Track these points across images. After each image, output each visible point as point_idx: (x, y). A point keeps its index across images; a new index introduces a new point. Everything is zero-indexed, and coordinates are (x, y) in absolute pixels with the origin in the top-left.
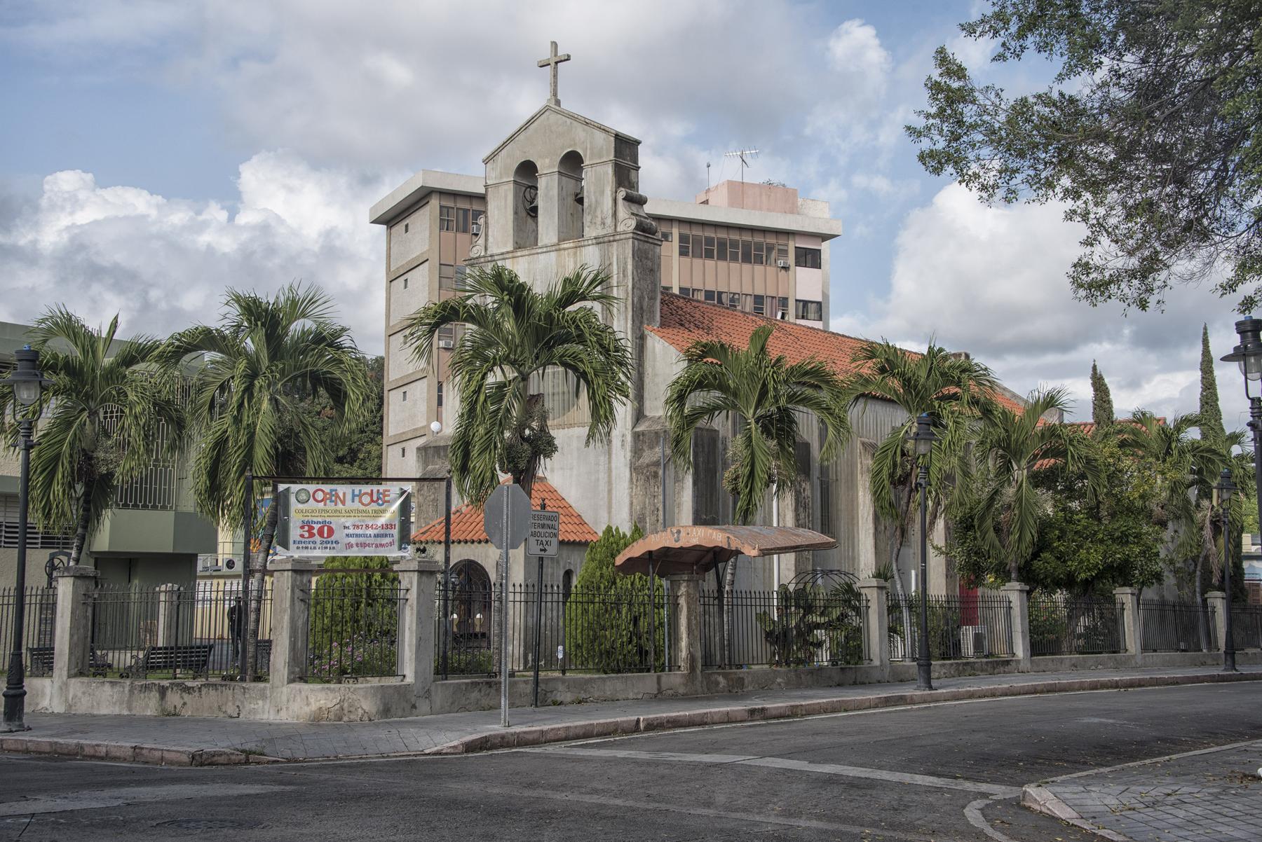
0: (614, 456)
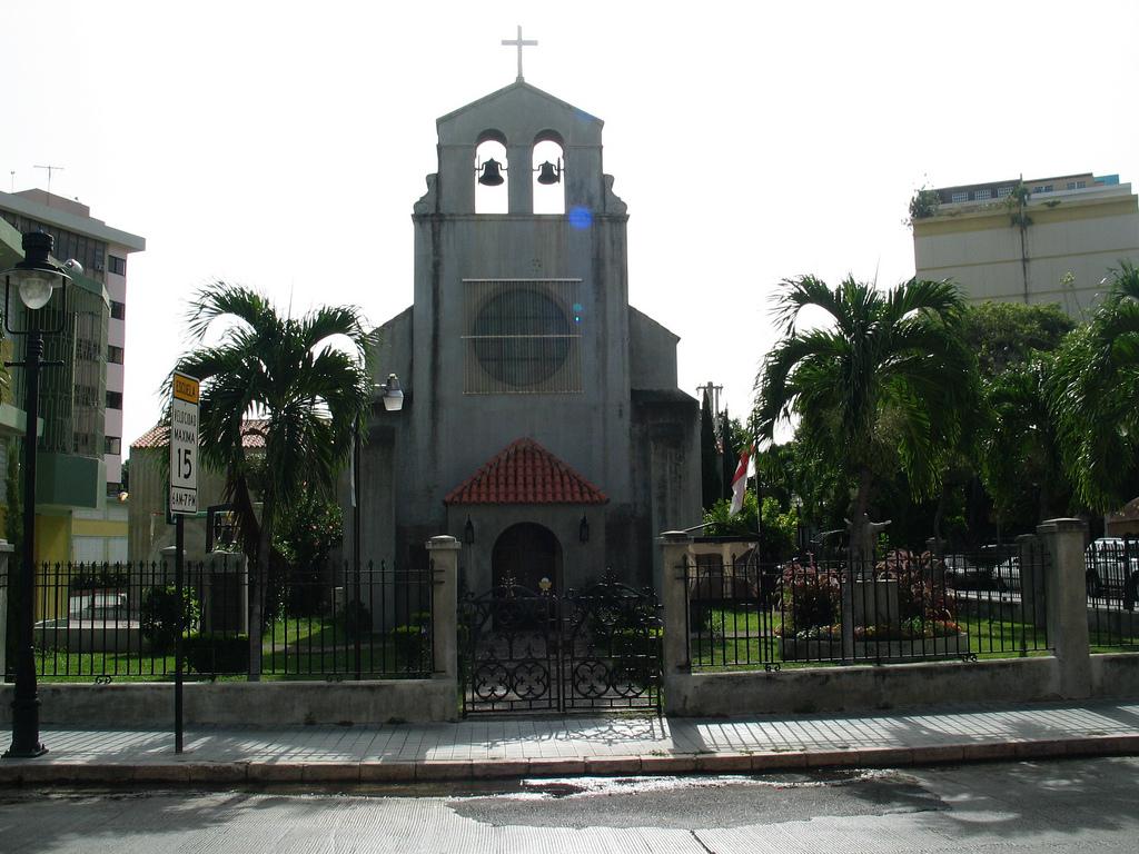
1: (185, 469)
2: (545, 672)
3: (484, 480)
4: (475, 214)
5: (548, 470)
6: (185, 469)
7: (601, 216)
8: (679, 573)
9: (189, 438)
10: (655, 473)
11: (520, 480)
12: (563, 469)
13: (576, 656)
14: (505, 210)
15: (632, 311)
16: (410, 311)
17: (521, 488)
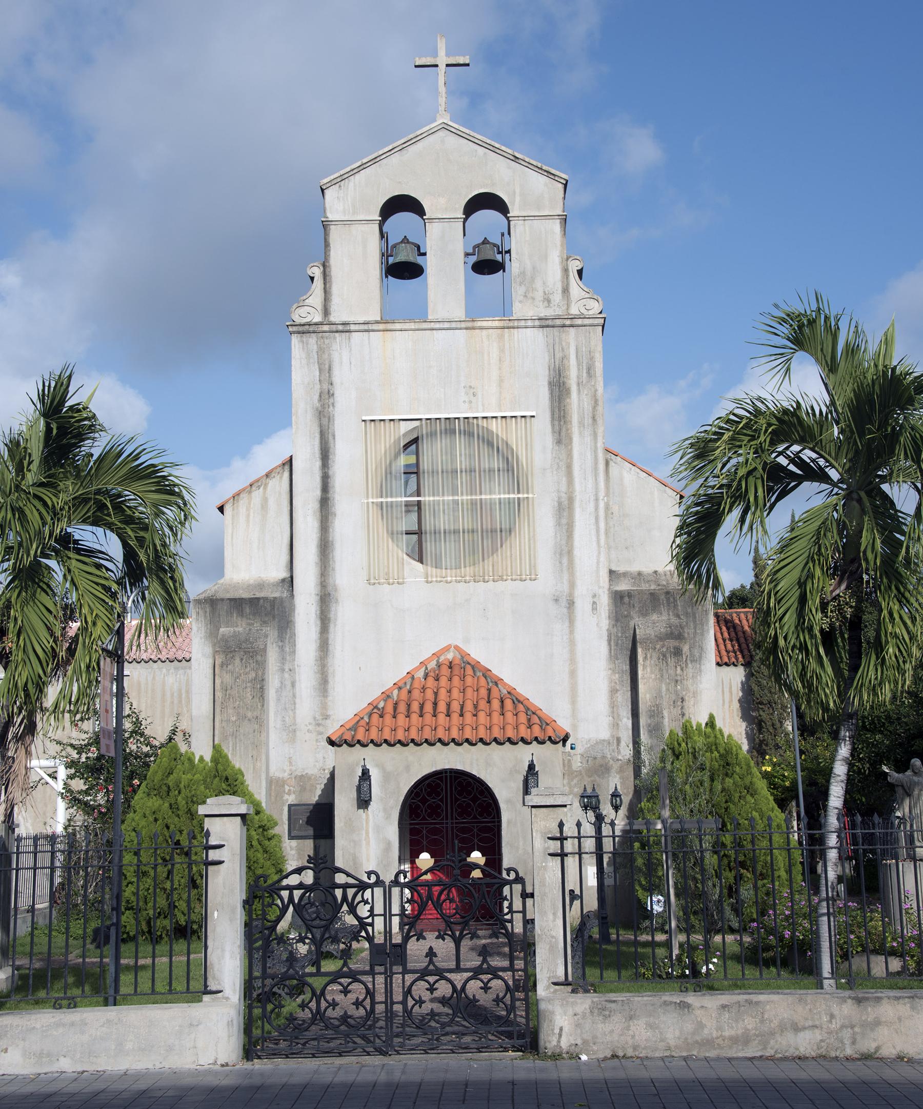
0: (578, 624)
2: (333, 981)
3: (389, 709)
8: (555, 846)
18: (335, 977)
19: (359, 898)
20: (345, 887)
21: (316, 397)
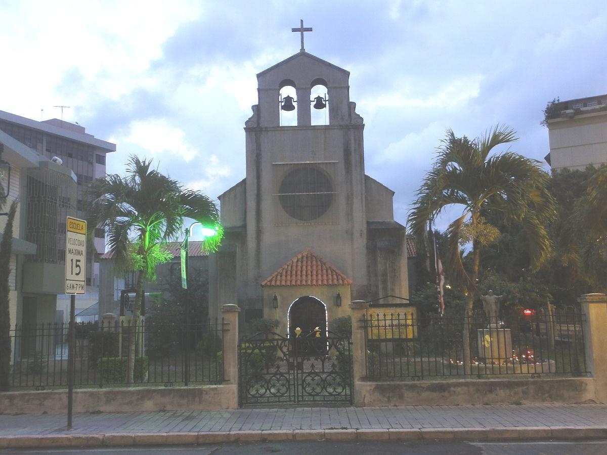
1: (76, 270)
2: (309, 375)
3: (284, 273)
4: (279, 127)
5: (320, 267)
6: (76, 270)
7: (349, 125)
8: (226, 328)
9: (79, 253)
10: (380, 268)
11: (304, 273)
12: (328, 267)
13: (304, 371)
14: (328, 124)
15: (367, 178)
16: (244, 181)
17: (304, 277)
18: (275, 375)
19: (283, 345)
20: (277, 340)
21: (255, 155)
